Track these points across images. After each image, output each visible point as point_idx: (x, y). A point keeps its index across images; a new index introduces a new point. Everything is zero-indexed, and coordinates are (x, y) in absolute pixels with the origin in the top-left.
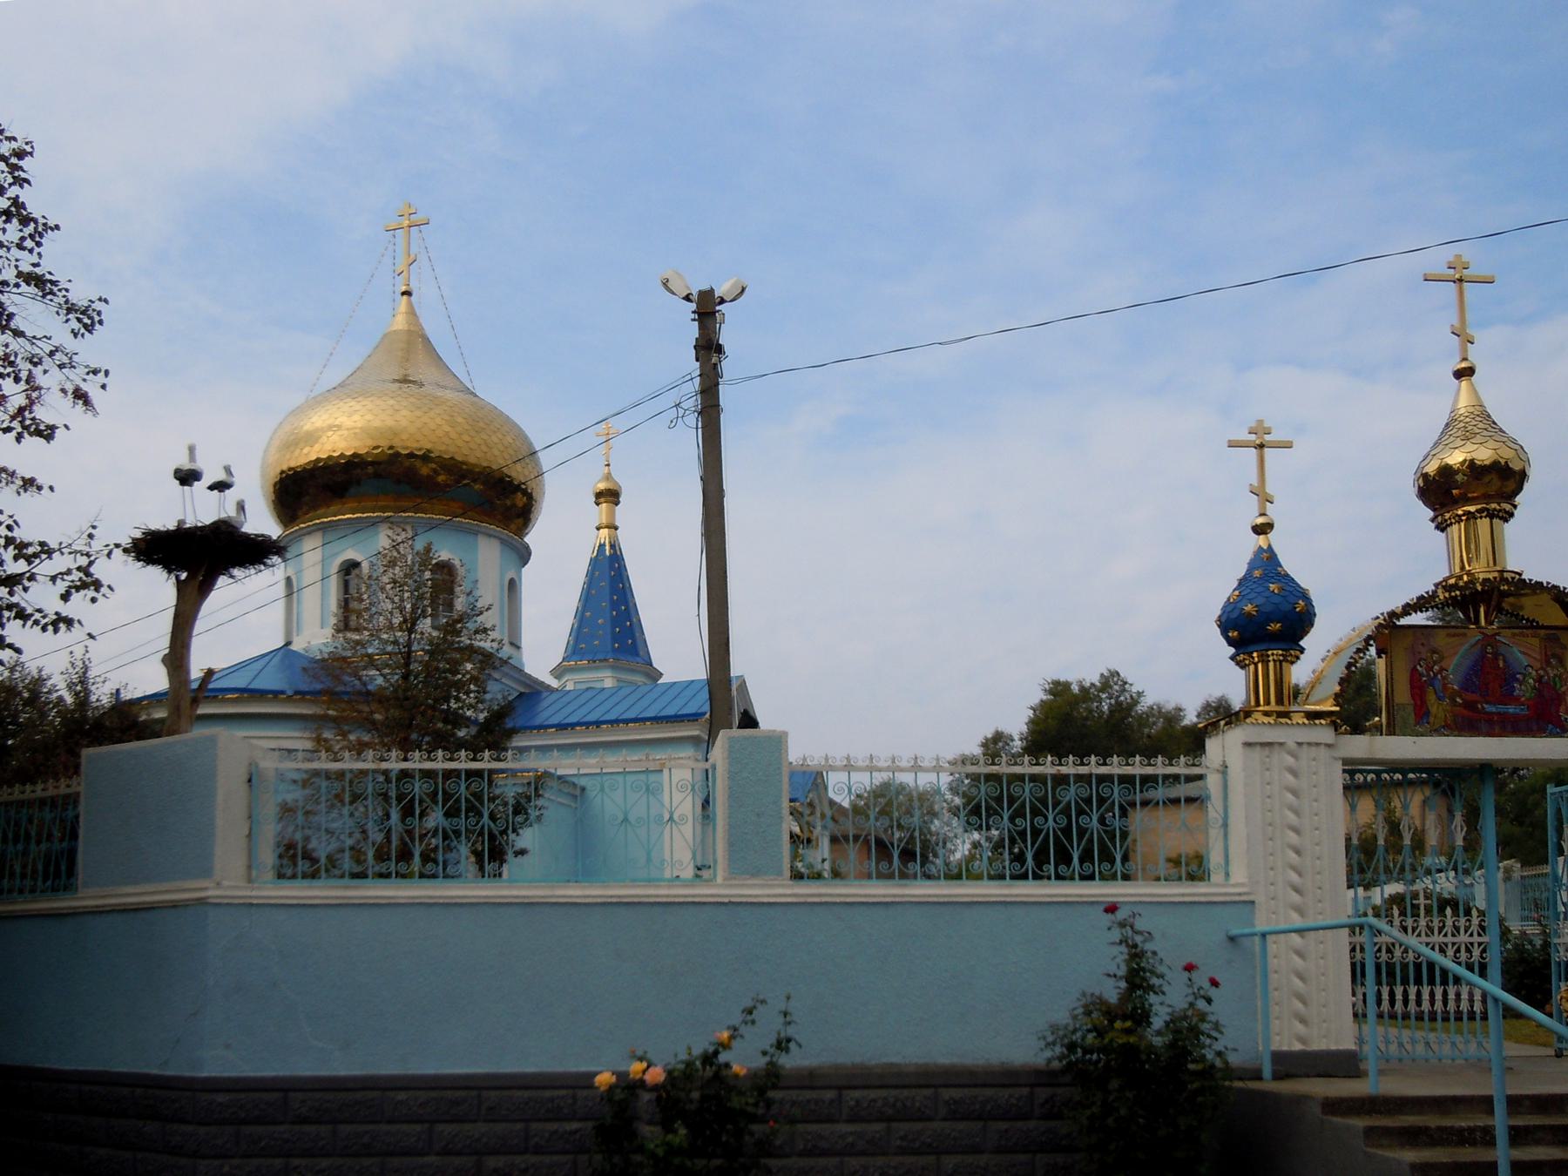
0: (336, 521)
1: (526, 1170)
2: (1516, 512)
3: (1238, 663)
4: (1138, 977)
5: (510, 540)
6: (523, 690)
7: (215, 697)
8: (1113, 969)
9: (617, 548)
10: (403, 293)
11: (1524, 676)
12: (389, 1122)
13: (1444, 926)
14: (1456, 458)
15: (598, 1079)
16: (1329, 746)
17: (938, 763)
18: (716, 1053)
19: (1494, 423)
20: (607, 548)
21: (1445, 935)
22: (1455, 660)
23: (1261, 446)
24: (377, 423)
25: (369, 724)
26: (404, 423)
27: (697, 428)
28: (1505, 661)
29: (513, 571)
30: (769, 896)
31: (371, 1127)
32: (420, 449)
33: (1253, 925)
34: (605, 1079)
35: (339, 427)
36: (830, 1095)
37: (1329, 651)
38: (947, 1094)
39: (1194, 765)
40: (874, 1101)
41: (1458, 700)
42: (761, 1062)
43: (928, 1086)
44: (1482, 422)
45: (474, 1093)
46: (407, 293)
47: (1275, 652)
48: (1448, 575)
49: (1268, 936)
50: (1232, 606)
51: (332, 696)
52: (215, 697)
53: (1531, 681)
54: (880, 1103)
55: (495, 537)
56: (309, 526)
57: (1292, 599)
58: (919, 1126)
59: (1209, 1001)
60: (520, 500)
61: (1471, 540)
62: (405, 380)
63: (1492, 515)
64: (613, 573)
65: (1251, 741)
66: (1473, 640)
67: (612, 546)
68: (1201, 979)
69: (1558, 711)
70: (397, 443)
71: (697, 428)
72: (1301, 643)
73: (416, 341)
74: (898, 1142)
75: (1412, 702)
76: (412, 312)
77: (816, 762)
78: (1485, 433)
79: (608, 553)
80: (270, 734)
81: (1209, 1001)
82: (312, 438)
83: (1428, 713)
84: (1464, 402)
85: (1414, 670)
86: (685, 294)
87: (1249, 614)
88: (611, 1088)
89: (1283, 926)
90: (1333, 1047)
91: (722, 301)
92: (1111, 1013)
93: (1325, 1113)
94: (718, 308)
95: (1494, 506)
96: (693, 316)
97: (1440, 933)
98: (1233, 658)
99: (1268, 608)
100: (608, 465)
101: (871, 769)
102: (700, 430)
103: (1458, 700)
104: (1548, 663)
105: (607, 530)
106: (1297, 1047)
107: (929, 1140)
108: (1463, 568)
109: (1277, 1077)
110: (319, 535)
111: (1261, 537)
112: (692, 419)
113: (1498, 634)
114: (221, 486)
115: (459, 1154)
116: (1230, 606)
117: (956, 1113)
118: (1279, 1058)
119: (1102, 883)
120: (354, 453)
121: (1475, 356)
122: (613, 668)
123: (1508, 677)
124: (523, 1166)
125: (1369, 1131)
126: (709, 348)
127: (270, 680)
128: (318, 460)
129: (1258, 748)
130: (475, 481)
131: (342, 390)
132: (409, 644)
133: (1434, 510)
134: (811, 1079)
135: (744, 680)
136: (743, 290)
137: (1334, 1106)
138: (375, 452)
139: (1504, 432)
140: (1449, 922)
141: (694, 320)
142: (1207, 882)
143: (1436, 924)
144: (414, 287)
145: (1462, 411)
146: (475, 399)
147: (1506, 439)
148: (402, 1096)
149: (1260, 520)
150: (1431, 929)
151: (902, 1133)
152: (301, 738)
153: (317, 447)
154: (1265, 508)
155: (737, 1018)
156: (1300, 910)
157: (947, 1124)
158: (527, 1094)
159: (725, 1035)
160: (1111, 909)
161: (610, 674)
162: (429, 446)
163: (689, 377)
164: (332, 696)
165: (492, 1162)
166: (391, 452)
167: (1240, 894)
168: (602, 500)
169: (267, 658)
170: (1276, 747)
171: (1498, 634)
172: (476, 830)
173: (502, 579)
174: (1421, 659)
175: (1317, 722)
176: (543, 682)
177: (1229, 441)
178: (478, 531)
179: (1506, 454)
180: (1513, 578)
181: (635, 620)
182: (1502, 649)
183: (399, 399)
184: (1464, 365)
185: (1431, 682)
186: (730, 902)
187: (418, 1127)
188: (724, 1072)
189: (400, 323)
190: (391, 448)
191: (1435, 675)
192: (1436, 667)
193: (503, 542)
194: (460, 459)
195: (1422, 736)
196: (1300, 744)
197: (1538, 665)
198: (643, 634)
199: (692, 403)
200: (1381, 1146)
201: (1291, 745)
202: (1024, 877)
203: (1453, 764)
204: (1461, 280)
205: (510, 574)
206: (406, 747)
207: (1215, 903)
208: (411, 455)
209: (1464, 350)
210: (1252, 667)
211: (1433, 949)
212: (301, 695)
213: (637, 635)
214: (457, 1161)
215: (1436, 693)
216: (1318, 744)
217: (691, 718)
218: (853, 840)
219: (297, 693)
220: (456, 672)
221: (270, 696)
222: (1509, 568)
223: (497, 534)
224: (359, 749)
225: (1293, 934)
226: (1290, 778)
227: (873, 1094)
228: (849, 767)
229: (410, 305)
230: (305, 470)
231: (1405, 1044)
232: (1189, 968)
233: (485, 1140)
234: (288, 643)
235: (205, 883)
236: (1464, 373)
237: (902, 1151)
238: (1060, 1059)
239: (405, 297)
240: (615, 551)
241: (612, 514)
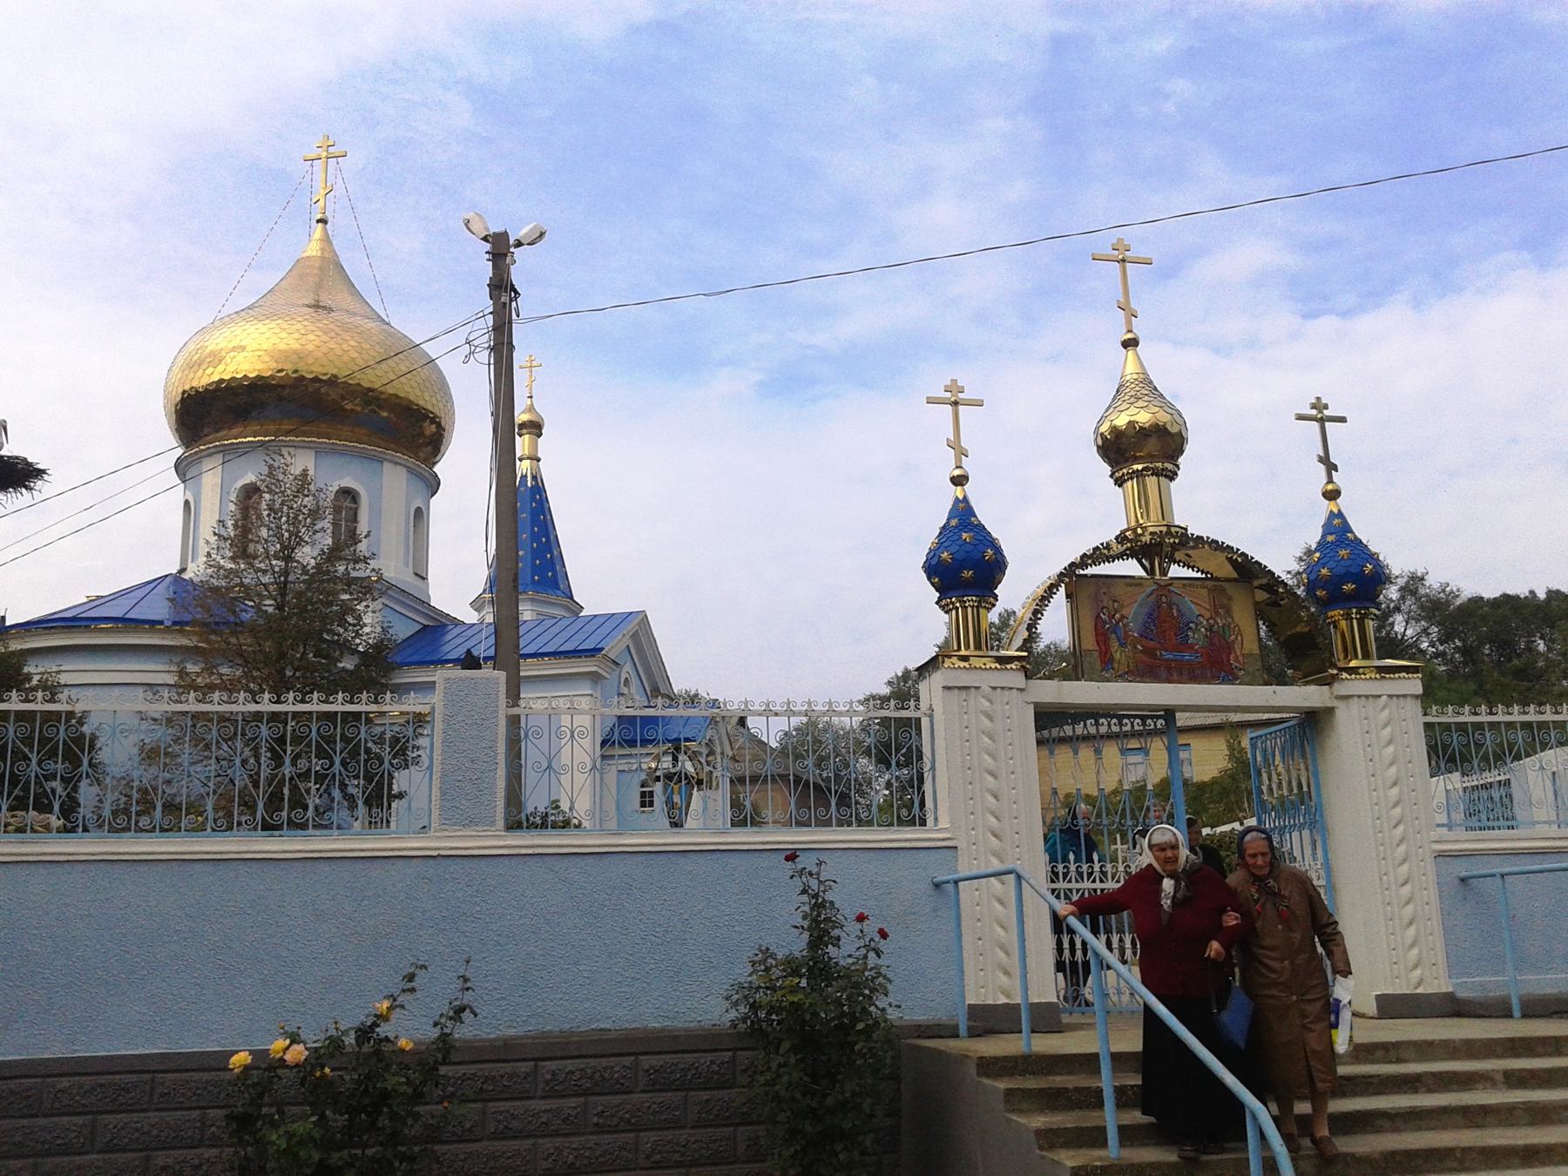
0: (237, 444)
1: (197, 1167)
2: (1179, 473)
3: (942, 608)
4: (821, 926)
5: (417, 468)
6: (426, 623)
7: (89, 626)
8: (799, 921)
10: (318, 221)
11: (1197, 625)
12: (45, 1116)
13: (1068, 872)
14: (1122, 421)
15: (234, 1059)
16: (1021, 690)
17: (788, 706)
18: (375, 1025)
19: (1155, 389)
20: (529, 479)
21: (1070, 881)
23: (956, 403)
24: (282, 347)
25: (238, 656)
26: (310, 347)
27: (489, 364)
28: (1178, 611)
29: (420, 500)
30: (479, 848)
31: (24, 1122)
32: (325, 374)
33: (956, 871)
34: (241, 1059)
35: (243, 348)
36: (524, 1067)
37: (1028, 598)
38: (647, 1062)
39: (903, 708)
40: (571, 1072)
41: (1139, 647)
42: (434, 1033)
43: (629, 1054)
44: (1146, 388)
45: (147, 1077)
46: (323, 221)
47: (970, 598)
48: (1126, 527)
49: (961, 884)
50: (932, 553)
51: (206, 628)
52: (89, 626)
53: (1203, 630)
54: (577, 1075)
55: (401, 464)
56: (209, 448)
57: (981, 547)
58: (616, 1099)
59: (878, 954)
61: (1143, 495)
62: (316, 306)
63: (1157, 473)
64: (534, 504)
65: (950, 685)
66: (1149, 590)
67: (534, 478)
68: (871, 928)
69: (1229, 660)
70: (301, 366)
71: (489, 364)
72: (996, 591)
73: (330, 268)
74: (595, 1120)
75: (1097, 648)
76: (327, 239)
77: (736, 707)
78: (1146, 398)
79: (529, 485)
81: (878, 954)
82: (216, 358)
83: (1112, 659)
84: (1131, 368)
85: (1098, 616)
86: (483, 235)
87: (945, 560)
88: (247, 1068)
89: (983, 871)
91: (519, 244)
92: (792, 967)
93: (979, 1074)
94: (512, 250)
95: (1159, 465)
96: (487, 256)
97: (1113, 879)
99: (959, 556)
100: (531, 397)
101: (790, 713)
102: (492, 367)
103: (1139, 647)
104: (1217, 614)
106: (1002, 1000)
107: (628, 1116)
108: (1138, 521)
109: (974, 1033)
110: (219, 458)
111: (959, 488)
112: (484, 356)
113: (1171, 585)
115: (124, 1150)
116: (933, 554)
117: (657, 1082)
118: (975, 1011)
119: (755, 829)
120: (232, 378)
121: (1139, 331)
123: (1183, 627)
124: (196, 1162)
125: (1009, 1093)
126: (502, 287)
127: (158, 609)
128: (222, 381)
129: (956, 691)
130: (381, 407)
131: (254, 311)
132: (286, 573)
133: (1112, 466)
134: (504, 1051)
135: (646, 616)
136: (542, 235)
137: (990, 1066)
138: (279, 375)
139: (1165, 398)
141: (489, 260)
142: (385, 830)
143: (1085, 867)
144: (329, 215)
145: (1128, 378)
146: (385, 327)
147: (1163, 405)
148: (65, 1083)
149: (957, 472)
150: (1080, 874)
151: (600, 1109)
152: (168, 671)
153: (221, 368)
154: (961, 461)
155: (395, 983)
156: (998, 855)
157: (645, 1096)
158: (206, 1076)
159: (386, 1004)
160: (792, 857)
162: (334, 371)
163: (481, 314)
164: (206, 628)
165: (161, 1158)
166: (294, 375)
167: (943, 840)
168: (524, 431)
170: (973, 690)
171: (1171, 585)
172: (328, 775)
173: (408, 507)
174: (1102, 608)
175: (1008, 666)
176: (1507, 600)
177: (928, 398)
178: (385, 459)
179: (1163, 418)
180: (1177, 533)
181: (555, 553)
182: (1175, 599)
183: (306, 323)
184: (1130, 336)
185: (1114, 629)
186: (439, 855)
187: (80, 1120)
188: (386, 1048)
189: (313, 249)
190: (296, 371)
191: (1117, 623)
192: (1117, 615)
193: (410, 470)
194: (366, 385)
195: (1109, 681)
196: (994, 688)
197: (1207, 615)
198: (564, 567)
199: (485, 340)
200: (1020, 1111)
201: (985, 688)
203: (1085, 708)
204: (1124, 260)
205: (418, 503)
206: (279, 688)
207: (474, 856)
208: (316, 380)
209: (1129, 322)
210: (954, 612)
211: (1058, 897)
212: (178, 625)
213: (558, 568)
214: (121, 1158)
215: (1119, 640)
216: (1011, 688)
217: (589, 654)
218: (750, 781)
219: (175, 623)
220: (330, 604)
222: (1176, 523)
223: (403, 462)
224: (230, 687)
225: (992, 879)
226: (986, 721)
227: (570, 1065)
228: (768, 712)
229: (325, 231)
230: (206, 390)
231: (1111, 995)
232: (861, 918)
233: (155, 1132)
234: (183, 570)
236: (1131, 343)
237: (600, 1129)
238: (744, 1020)
239: (320, 225)
240: (537, 482)
241: (535, 446)
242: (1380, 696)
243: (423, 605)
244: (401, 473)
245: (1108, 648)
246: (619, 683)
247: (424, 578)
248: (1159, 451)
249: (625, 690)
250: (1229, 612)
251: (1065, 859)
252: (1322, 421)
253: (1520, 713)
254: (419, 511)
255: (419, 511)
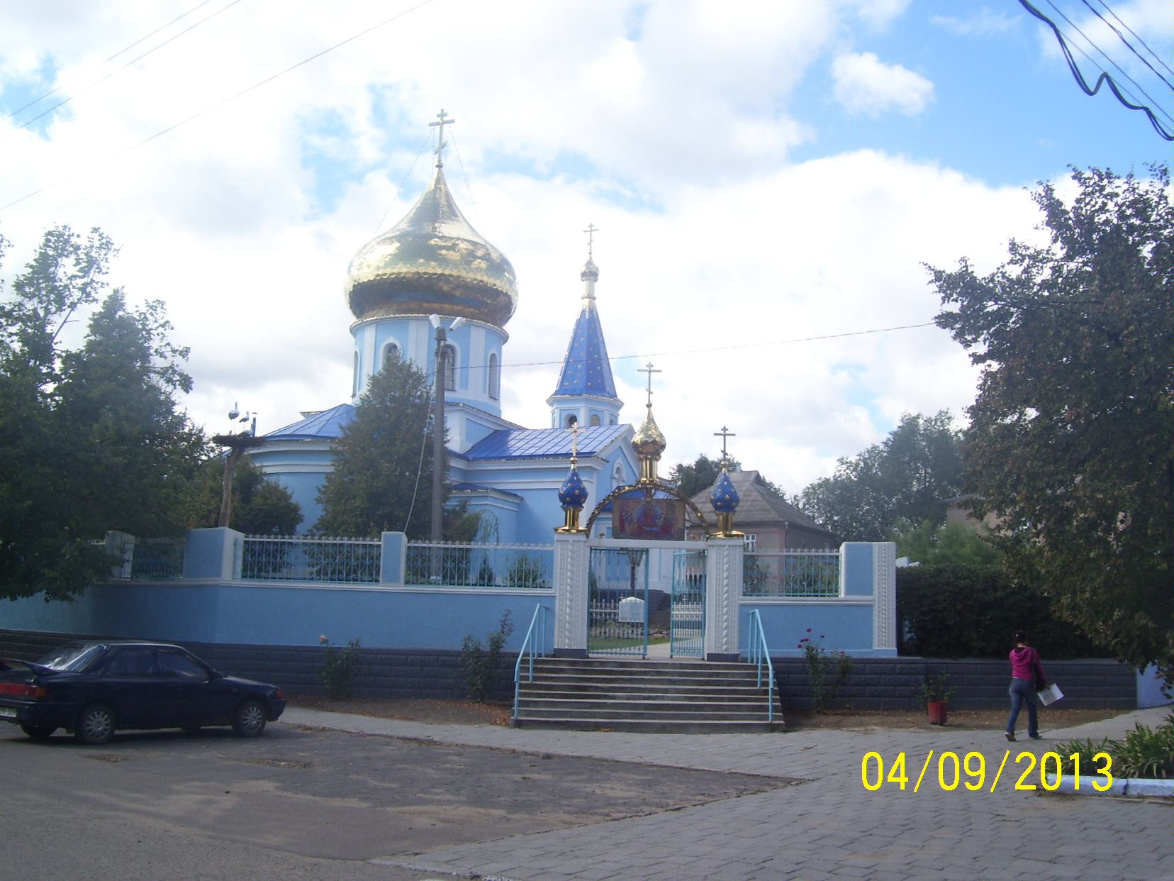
9: (595, 312)
22: (636, 511)
36: (403, 657)
60: (501, 299)
80: (319, 463)
83: (625, 530)
85: (621, 515)
90: (578, 648)
98: (562, 507)
105: (588, 299)
114: (244, 420)
122: (586, 400)
140: (604, 605)
143: (599, 605)
161: (584, 405)
169: (333, 412)
193: (488, 330)
198: (611, 374)
202: (483, 585)
221: (329, 440)
235: (218, 579)
240: (593, 315)
242: (725, 546)
243: (497, 418)
244: (482, 332)
245: (624, 527)
246: (612, 471)
247: (496, 399)
248: (1139, 250)
249: (616, 476)
250: (674, 512)
251: (601, 601)
252: (725, 435)
253: (793, 552)
254: (493, 356)
255: (493, 356)
